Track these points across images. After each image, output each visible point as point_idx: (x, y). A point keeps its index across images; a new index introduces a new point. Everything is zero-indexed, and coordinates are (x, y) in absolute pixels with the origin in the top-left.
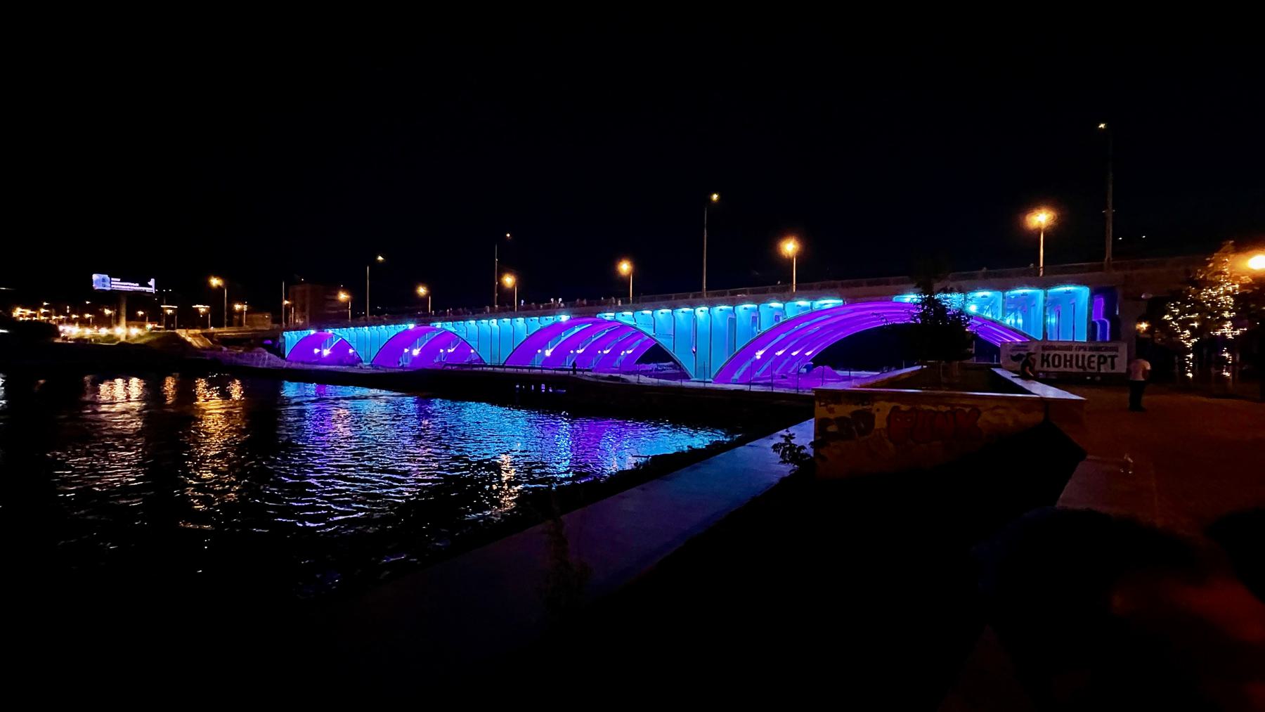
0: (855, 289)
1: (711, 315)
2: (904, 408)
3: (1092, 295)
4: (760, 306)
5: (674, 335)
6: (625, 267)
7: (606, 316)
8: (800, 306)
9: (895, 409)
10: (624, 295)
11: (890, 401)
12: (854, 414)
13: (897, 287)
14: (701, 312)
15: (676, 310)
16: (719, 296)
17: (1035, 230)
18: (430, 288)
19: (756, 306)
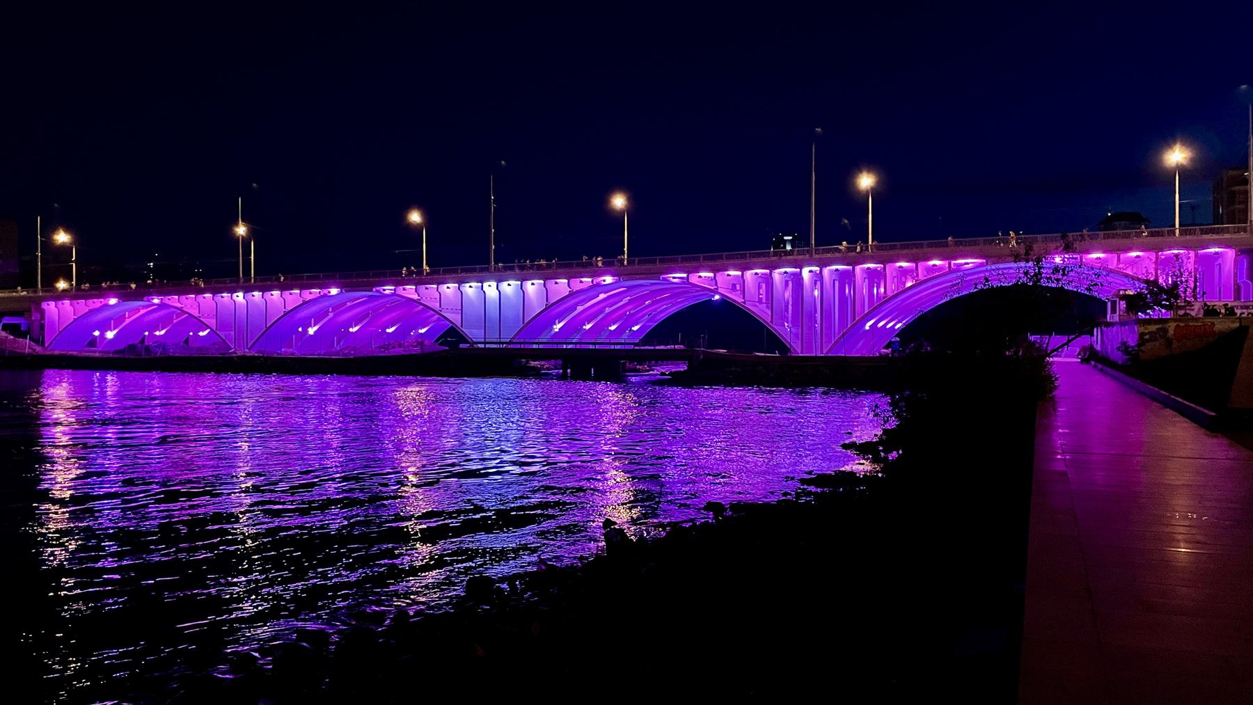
0: (915, 251)
1: (499, 291)
2: (1182, 325)
3: (1237, 255)
4: (571, 281)
5: (462, 310)
6: (619, 202)
7: (384, 290)
8: (902, 267)
9: (1177, 326)
10: (611, 253)
11: (1175, 322)
12: (1157, 329)
13: (892, 252)
14: (491, 289)
15: (463, 285)
16: (917, 248)
17: (865, 192)
18: (632, 199)
19: (914, 265)
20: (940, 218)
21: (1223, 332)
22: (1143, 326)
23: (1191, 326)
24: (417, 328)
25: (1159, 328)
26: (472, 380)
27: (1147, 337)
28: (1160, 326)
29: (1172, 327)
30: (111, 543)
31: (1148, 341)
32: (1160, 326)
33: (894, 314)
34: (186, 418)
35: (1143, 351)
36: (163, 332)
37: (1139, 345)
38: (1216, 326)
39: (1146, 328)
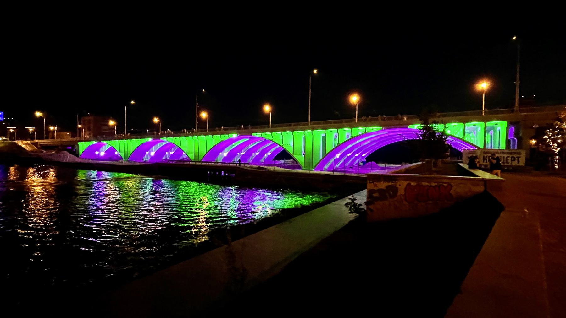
9: (409, 184)
18: (210, 114)
20: (64, 243)
25: (389, 186)
26: (112, 164)
28: (390, 184)
29: (402, 185)
31: (377, 199)
38: (454, 188)
39: (376, 186)
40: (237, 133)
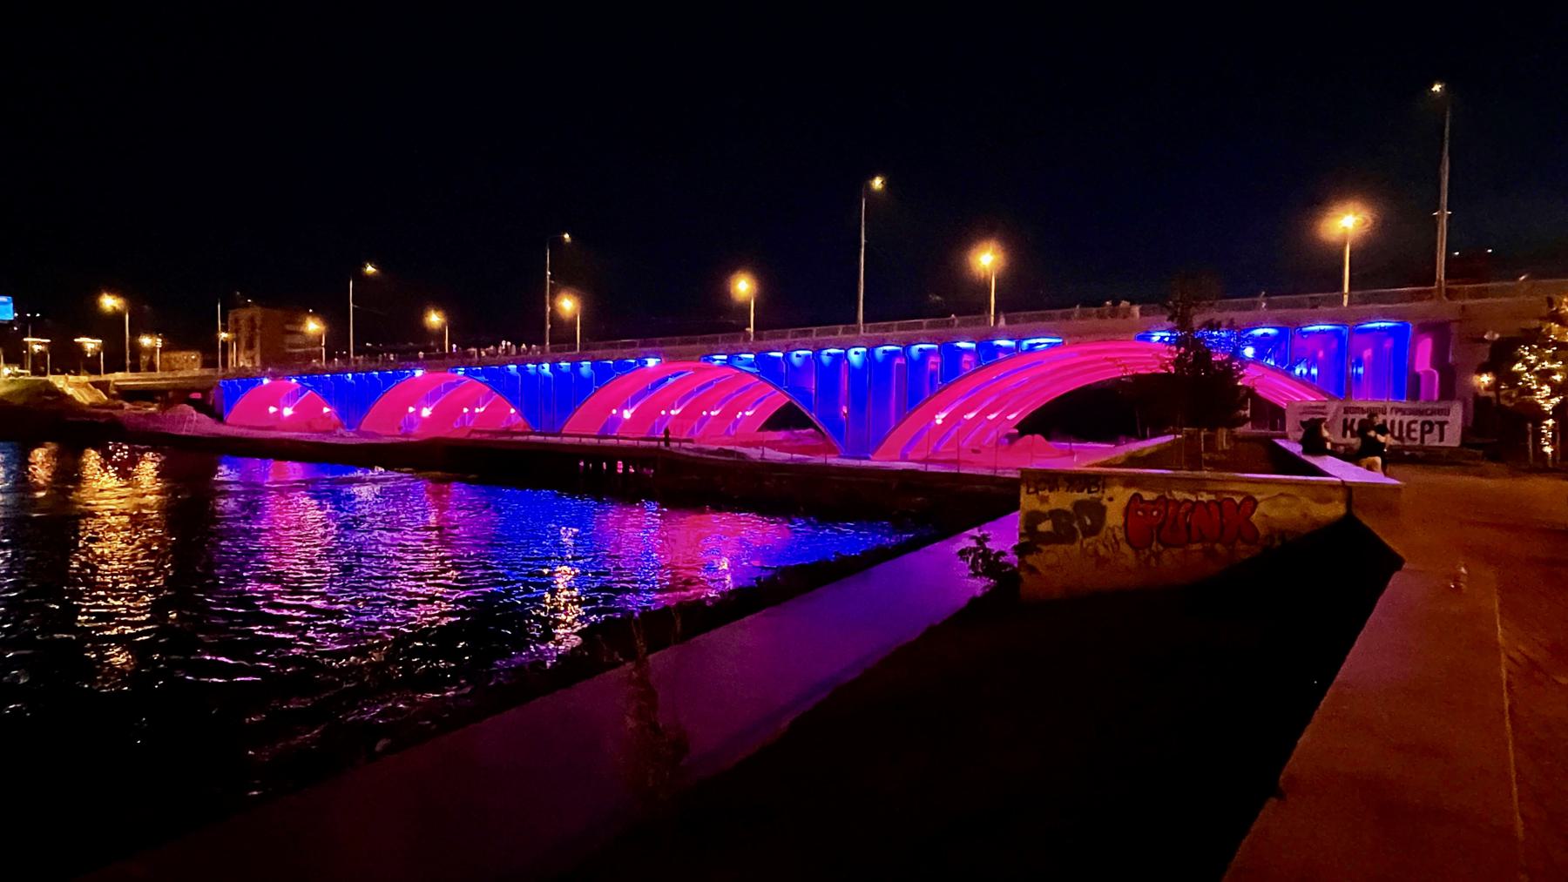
2: (1148, 496)
9: (1136, 497)
21: (1282, 533)
22: (1036, 492)
23: (1178, 504)
24: (744, 411)
27: (1045, 526)
28: (1084, 496)
29: (1116, 500)
30: (312, 616)
31: (1049, 538)
32: (1084, 496)
33: (1004, 408)
34: (972, 463)
35: (1032, 570)
36: (482, 409)
37: (1021, 550)
40: (649, 368)
